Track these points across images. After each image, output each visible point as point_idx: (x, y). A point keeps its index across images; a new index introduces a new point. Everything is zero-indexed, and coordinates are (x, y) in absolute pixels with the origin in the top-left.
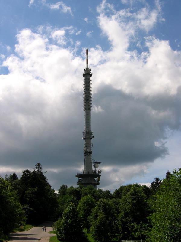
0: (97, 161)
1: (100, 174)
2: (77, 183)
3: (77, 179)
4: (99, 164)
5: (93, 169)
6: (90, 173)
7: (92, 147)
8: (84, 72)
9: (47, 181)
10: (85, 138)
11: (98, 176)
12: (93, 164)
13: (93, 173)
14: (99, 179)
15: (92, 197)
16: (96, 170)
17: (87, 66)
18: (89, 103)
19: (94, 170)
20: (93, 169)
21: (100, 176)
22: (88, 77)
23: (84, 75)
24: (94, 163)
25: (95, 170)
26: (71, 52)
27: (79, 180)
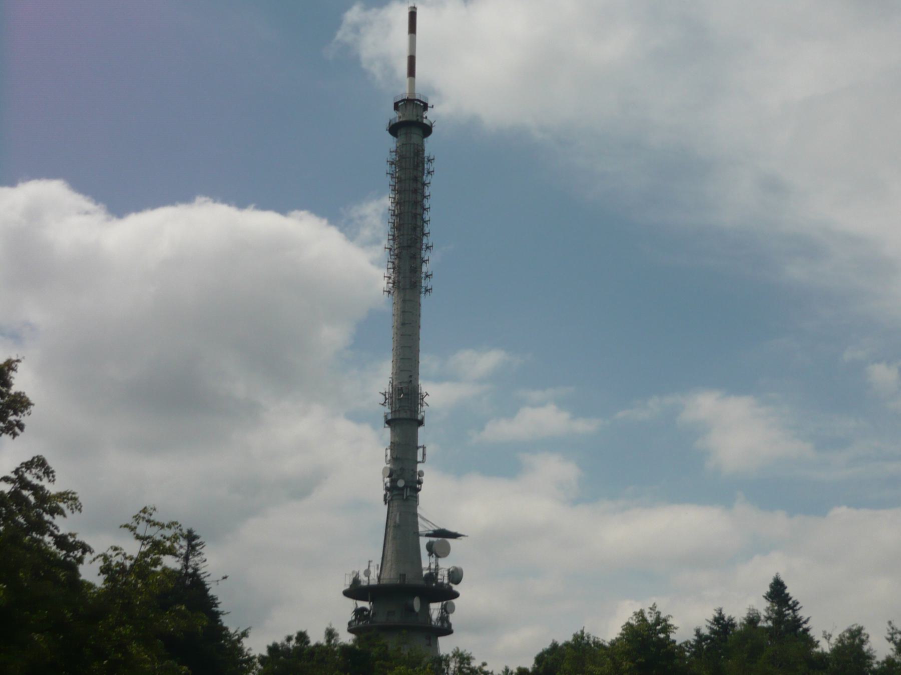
0: (442, 527)
1: (455, 588)
2: (350, 624)
3: (351, 605)
4: (451, 541)
5: (425, 562)
6: (411, 580)
7: (423, 462)
8: (394, 116)
9: (222, 617)
10: (389, 417)
11: (447, 595)
12: (423, 542)
13: (422, 583)
14: (446, 611)
15: (432, 657)
16: (437, 565)
17: (412, 85)
18: (415, 216)
19: (429, 568)
20: (426, 562)
21: (456, 595)
22: (415, 138)
23: (394, 129)
24: (428, 535)
25: (433, 566)
26: (361, 218)
27: (359, 612)
